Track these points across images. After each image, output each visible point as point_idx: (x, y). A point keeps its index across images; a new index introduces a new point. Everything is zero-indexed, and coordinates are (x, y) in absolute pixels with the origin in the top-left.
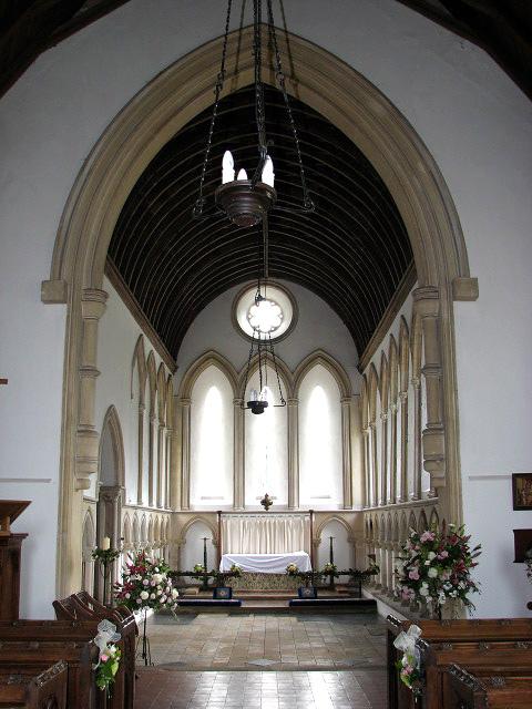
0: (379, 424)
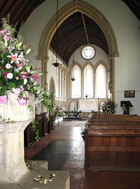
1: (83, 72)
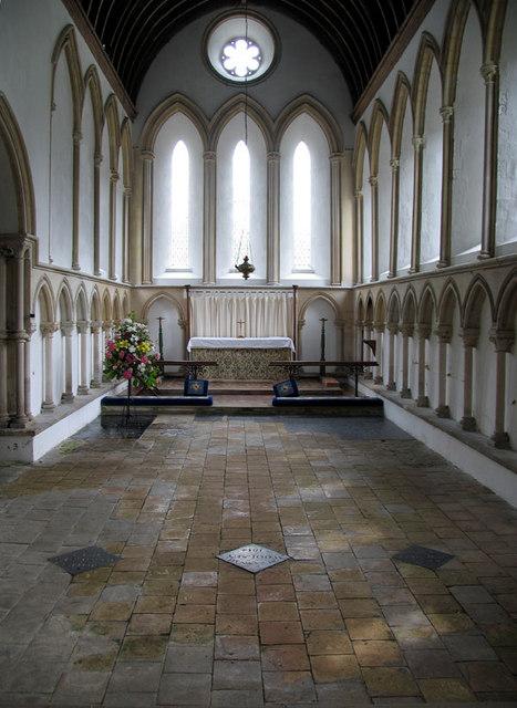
1: (214, 150)
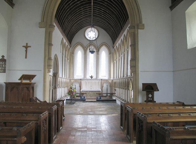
0: (118, 60)
1: (86, 53)
